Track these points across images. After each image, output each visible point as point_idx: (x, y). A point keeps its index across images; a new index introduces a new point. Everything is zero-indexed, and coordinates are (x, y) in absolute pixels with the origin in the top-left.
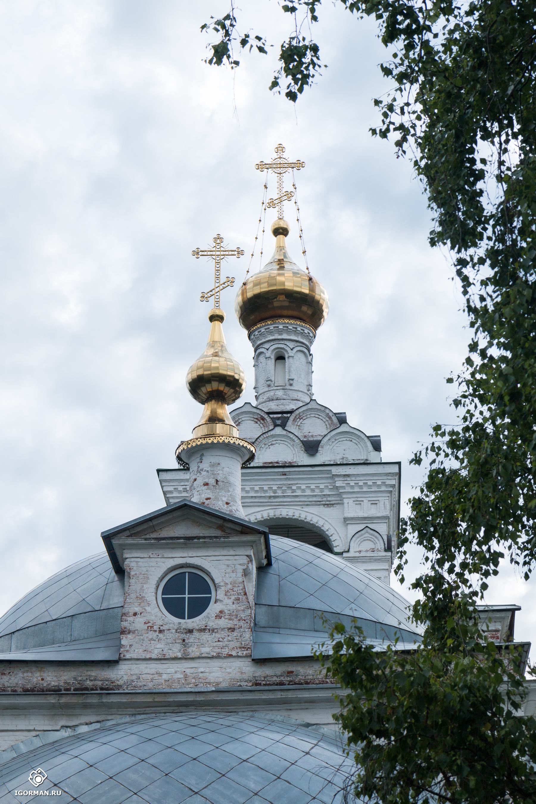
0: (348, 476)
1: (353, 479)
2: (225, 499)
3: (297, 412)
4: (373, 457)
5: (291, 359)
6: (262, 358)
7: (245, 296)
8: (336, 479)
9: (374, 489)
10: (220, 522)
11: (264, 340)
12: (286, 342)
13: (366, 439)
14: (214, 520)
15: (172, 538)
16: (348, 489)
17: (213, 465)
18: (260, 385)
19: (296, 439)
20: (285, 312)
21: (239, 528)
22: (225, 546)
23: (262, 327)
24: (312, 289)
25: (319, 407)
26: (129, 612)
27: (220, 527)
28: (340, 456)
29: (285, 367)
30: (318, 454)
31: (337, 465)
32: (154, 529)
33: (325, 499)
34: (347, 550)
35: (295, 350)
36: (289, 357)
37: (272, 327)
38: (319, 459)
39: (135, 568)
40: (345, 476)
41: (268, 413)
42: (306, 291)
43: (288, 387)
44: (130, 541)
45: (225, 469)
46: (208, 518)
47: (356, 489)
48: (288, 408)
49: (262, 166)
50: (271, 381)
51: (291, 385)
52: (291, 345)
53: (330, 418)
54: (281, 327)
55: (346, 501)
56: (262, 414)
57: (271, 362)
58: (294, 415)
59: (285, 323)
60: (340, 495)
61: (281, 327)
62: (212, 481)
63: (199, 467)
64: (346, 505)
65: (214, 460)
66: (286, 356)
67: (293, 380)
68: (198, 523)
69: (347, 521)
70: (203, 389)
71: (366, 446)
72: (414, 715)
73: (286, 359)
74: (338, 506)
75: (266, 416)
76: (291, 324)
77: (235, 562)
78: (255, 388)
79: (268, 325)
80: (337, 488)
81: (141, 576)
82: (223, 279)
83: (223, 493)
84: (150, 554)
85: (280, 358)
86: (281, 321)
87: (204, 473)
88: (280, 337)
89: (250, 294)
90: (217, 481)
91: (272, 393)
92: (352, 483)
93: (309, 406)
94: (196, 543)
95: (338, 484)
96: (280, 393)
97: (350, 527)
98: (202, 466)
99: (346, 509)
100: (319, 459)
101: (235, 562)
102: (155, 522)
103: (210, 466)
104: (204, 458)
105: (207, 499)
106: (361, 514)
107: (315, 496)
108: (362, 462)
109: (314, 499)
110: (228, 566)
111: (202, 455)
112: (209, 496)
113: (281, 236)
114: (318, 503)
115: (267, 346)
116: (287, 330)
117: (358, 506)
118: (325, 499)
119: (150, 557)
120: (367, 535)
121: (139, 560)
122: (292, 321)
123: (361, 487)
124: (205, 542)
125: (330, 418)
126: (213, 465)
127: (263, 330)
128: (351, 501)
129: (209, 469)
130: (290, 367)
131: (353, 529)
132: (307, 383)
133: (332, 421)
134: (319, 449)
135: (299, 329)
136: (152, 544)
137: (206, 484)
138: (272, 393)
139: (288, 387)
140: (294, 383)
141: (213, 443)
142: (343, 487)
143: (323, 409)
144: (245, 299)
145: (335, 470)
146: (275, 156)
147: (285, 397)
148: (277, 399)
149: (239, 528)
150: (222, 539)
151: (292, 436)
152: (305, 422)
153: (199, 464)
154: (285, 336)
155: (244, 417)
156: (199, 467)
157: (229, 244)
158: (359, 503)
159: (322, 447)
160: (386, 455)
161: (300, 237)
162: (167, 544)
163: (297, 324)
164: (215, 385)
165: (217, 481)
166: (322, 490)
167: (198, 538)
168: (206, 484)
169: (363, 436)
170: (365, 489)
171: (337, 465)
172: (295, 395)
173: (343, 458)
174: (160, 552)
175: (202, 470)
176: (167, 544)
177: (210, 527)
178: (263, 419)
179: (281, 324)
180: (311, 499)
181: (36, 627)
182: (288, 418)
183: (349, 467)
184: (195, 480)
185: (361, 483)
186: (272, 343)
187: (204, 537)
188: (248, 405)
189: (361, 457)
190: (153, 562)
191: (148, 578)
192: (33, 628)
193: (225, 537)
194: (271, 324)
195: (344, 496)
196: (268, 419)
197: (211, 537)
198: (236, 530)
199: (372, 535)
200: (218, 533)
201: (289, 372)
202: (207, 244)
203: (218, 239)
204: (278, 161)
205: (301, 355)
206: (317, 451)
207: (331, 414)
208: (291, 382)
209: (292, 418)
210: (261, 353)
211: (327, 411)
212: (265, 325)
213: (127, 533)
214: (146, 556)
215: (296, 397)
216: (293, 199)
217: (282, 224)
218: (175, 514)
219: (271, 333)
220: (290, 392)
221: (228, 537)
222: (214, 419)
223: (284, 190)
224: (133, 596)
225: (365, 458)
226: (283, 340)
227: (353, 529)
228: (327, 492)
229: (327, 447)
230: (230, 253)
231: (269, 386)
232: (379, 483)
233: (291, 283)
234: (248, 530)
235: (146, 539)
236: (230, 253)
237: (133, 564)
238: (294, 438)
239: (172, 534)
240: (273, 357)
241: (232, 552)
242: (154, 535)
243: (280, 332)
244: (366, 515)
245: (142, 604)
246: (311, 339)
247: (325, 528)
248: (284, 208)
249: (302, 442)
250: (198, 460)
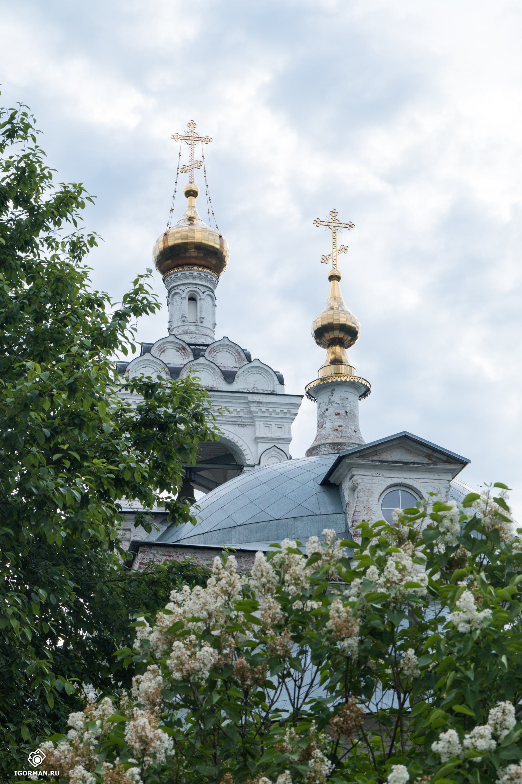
0: (261, 403)
1: (265, 405)
2: (353, 428)
3: (212, 346)
4: (278, 389)
5: (202, 301)
6: (177, 298)
7: (166, 244)
8: (251, 405)
9: (281, 415)
10: (429, 452)
11: (179, 283)
12: (198, 286)
13: (273, 373)
14: (425, 449)
15: (393, 462)
16: (260, 414)
17: (342, 399)
18: (174, 320)
19: (217, 368)
20: (198, 262)
21: (444, 458)
22: (432, 471)
23: (179, 272)
24: (222, 245)
25: (231, 344)
26: (358, 520)
27: (428, 456)
28: (252, 386)
29: (196, 306)
30: (234, 383)
31: (249, 393)
32: (376, 453)
33: (240, 420)
34: (257, 463)
35: (206, 294)
36: (201, 299)
37: (187, 273)
38: (235, 387)
39: (361, 484)
40: (258, 402)
41: (189, 345)
42: (218, 247)
43: (200, 324)
44: (360, 461)
45: (352, 403)
46: (420, 448)
47: (267, 415)
48: (200, 341)
49: (176, 137)
50: (185, 317)
51: (202, 322)
52: (203, 289)
53: (239, 353)
54: (195, 273)
55: (257, 423)
56: (184, 345)
57: (186, 302)
58: (210, 348)
59: (199, 271)
60: (252, 418)
61: (195, 273)
62: (342, 412)
63: (330, 399)
64: (257, 426)
65: (344, 395)
66: (198, 298)
67: (203, 318)
68: (409, 451)
69: (257, 440)
70: (326, 335)
71: (273, 380)
72: (386, 606)
73: (198, 301)
74: (250, 427)
75: (187, 347)
76: (204, 272)
77: (440, 485)
78: (169, 322)
79: (185, 270)
80: (251, 412)
81: (367, 491)
82: (338, 247)
83: (351, 422)
84: (373, 473)
85: (192, 299)
86: (195, 268)
87: (335, 405)
88: (193, 282)
89: (171, 243)
90: (346, 412)
91: (186, 328)
92: (264, 409)
93: (222, 342)
94: (411, 467)
95: (253, 409)
96: (193, 329)
97: (259, 444)
98: (333, 399)
99: (257, 430)
100: (235, 387)
101: (440, 485)
102: (378, 448)
103: (340, 399)
104: (334, 392)
105: (339, 426)
106: (269, 435)
107: (233, 417)
108: (270, 392)
109: (231, 419)
110: (434, 487)
111: (333, 390)
112: (340, 424)
113: (192, 197)
114: (234, 423)
115: (181, 287)
116: (199, 277)
117: (267, 428)
118: (240, 420)
119: (373, 476)
120: (274, 453)
121: (364, 477)
122: (204, 270)
123: (270, 413)
124: (417, 467)
125: (239, 353)
126: (342, 399)
127: (179, 274)
128: (261, 423)
129: (340, 402)
130: (201, 308)
131: (263, 447)
132: (212, 322)
133: (240, 356)
134: (236, 378)
135: (209, 277)
136: (376, 465)
137: (338, 414)
138: (186, 328)
139: (200, 324)
140: (204, 320)
141: (346, 381)
142: (256, 412)
143: (233, 345)
144: (167, 246)
145: (251, 397)
146: (188, 130)
147: (197, 332)
148: (191, 333)
149: (444, 458)
150: (432, 466)
151: (213, 365)
152: (218, 354)
153: (331, 397)
154: (197, 281)
155: (168, 346)
156: (330, 399)
157: (343, 218)
158: (268, 426)
159: (238, 377)
160: (288, 389)
161: (174, 197)
162: (387, 466)
163: (208, 273)
164: (337, 334)
165: (346, 412)
166: (238, 413)
167: (414, 463)
168: (338, 414)
169: (271, 372)
170: (274, 415)
171: (249, 393)
172: (205, 331)
173: (254, 388)
174: (382, 472)
175: (334, 402)
176: (387, 466)
177: (419, 455)
178: (184, 349)
179: (196, 270)
180: (228, 419)
181: (259, 525)
182: (205, 350)
183: (262, 395)
184: (327, 410)
185: (271, 410)
186: (187, 286)
187: (418, 463)
188: (225, 339)
189: (269, 388)
190: (375, 480)
191: (372, 493)
192: (255, 525)
193: (434, 465)
194: (187, 271)
195: (256, 419)
196: (189, 350)
197: (423, 464)
198: (442, 459)
199: (278, 453)
200: (426, 460)
201: (201, 311)
202: (325, 216)
203: (334, 212)
204: (191, 134)
205: (209, 298)
206: (233, 380)
207: (240, 350)
208: (202, 320)
209: (208, 351)
210: (176, 293)
211: (237, 347)
212: (182, 271)
213: (358, 455)
214: (369, 474)
215: (205, 333)
216: (202, 168)
217: (193, 187)
218: (394, 443)
219: (186, 277)
220: (201, 328)
221: (436, 465)
222: (337, 361)
223: (195, 159)
224: (361, 506)
225: (272, 389)
226: (196, 284)
227: (263, 447)
228: (242, 415)
229: (241, 378)
230: (343, 225)
231: (184, 321)
232: (285, 411)
233: (199, 237)
234: (452, 460)
235: (372, 461)
236: (343, 225)
237: (360, 480)
238: (215, 367)
239: (389, 458)
240: (187, 298)
241: (437, 477)
242: (375, 458)
243: (194, 278)
244: (273, 436)
245: (369, 514)
246: (215, 284)
247: (239, 444)
248: (194, 175)
249: (223, 372)
250: (330, 394)
